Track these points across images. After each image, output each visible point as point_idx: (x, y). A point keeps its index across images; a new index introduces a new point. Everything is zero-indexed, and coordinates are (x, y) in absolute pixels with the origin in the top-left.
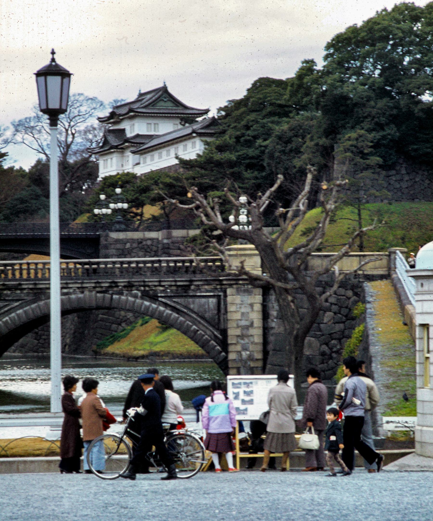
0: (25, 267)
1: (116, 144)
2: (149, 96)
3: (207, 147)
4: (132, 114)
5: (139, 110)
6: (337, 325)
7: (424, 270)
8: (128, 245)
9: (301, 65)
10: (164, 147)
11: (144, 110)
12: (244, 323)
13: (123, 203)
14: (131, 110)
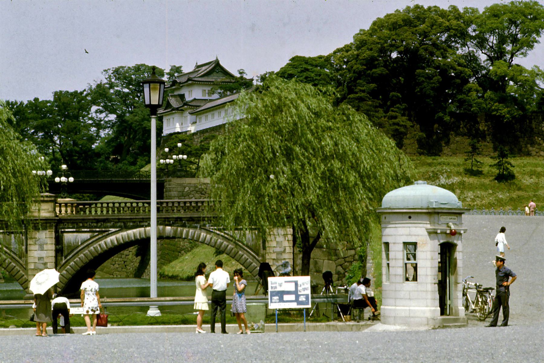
1: (177, 107)
2: (204, 68)
3: (294, 79)
4: (190, 82)
5: (196, 79)
6: (349, 251)
8: (187, 189)
9: (528, 52)
10: (216, 109)
11: (200, 79)
12: (278, 249)
13: (183, 154)
14: (189, 79)
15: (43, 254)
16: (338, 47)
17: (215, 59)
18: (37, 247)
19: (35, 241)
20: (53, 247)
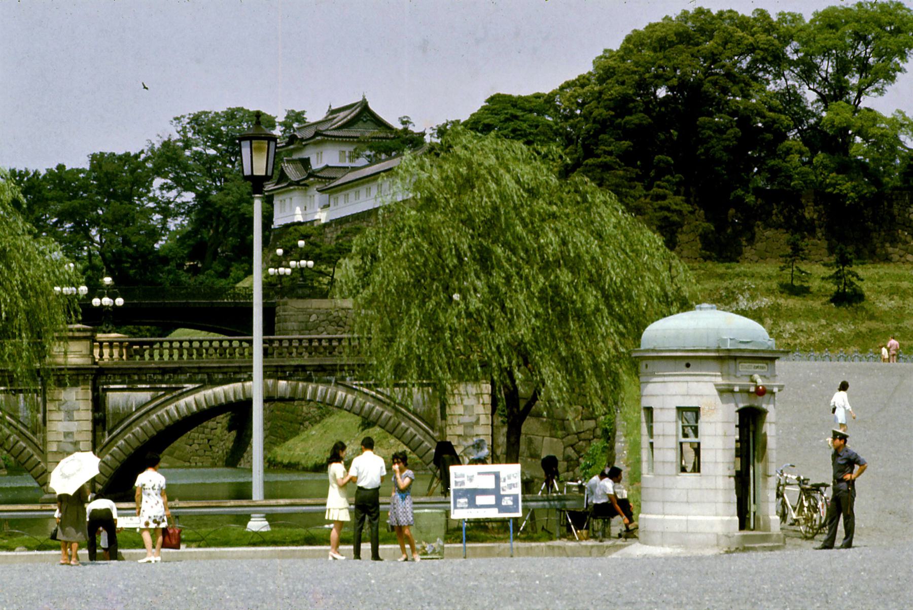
0: (286, 344)
1: (297, 179)
2: (342, 115)
4: (319, 138)
5: (329, 133)
6: (585, 422)
7: (676, 351)
8: (314, 317)
9: (887, 87)
10: (363, 183)
11: (336, 133)
12: (467, 419)
13: (307, 259)
14: (317, 134)
15: (73, 427)
16: (568, 79)
17: (360, 99)
18: (62, 415)
19: (59, 405)
20: (89, 416)
